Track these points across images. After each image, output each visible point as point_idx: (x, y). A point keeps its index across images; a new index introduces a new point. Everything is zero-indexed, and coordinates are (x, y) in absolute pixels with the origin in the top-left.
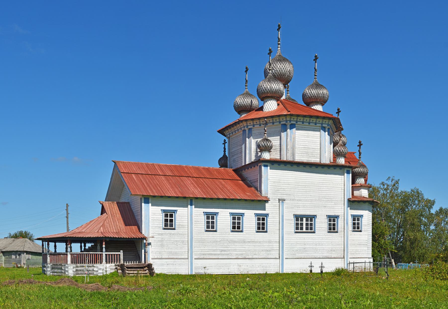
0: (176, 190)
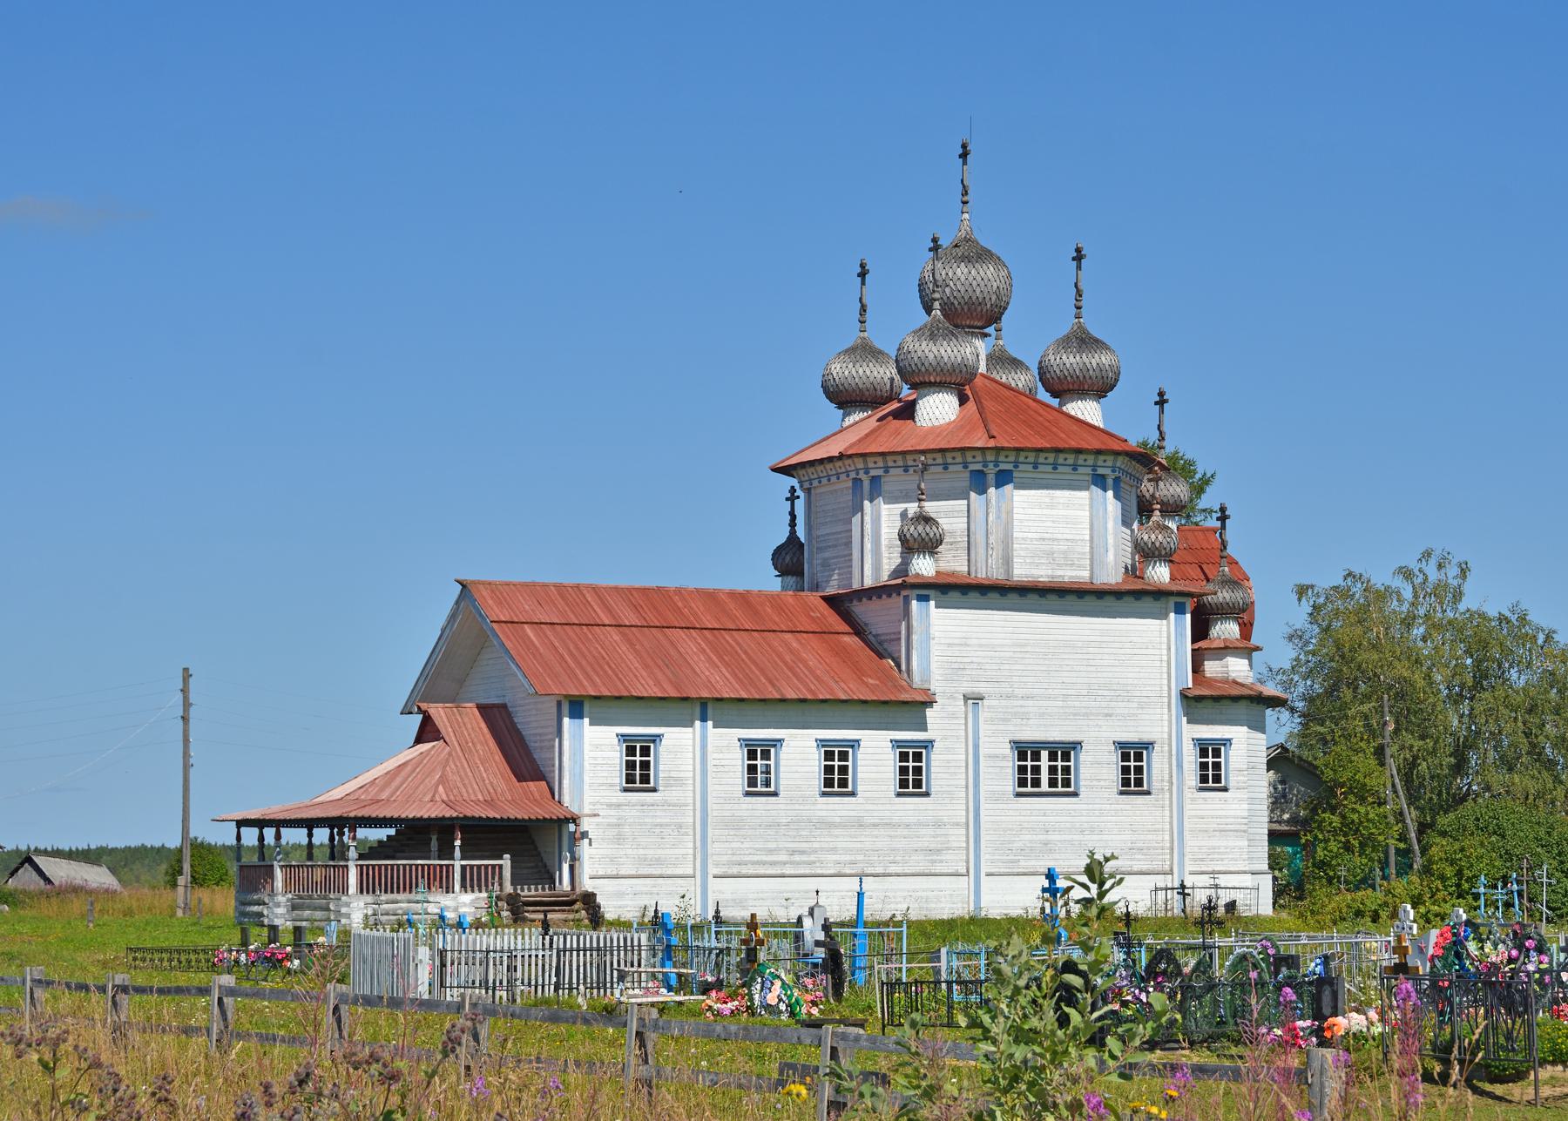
0: (660, 675)
